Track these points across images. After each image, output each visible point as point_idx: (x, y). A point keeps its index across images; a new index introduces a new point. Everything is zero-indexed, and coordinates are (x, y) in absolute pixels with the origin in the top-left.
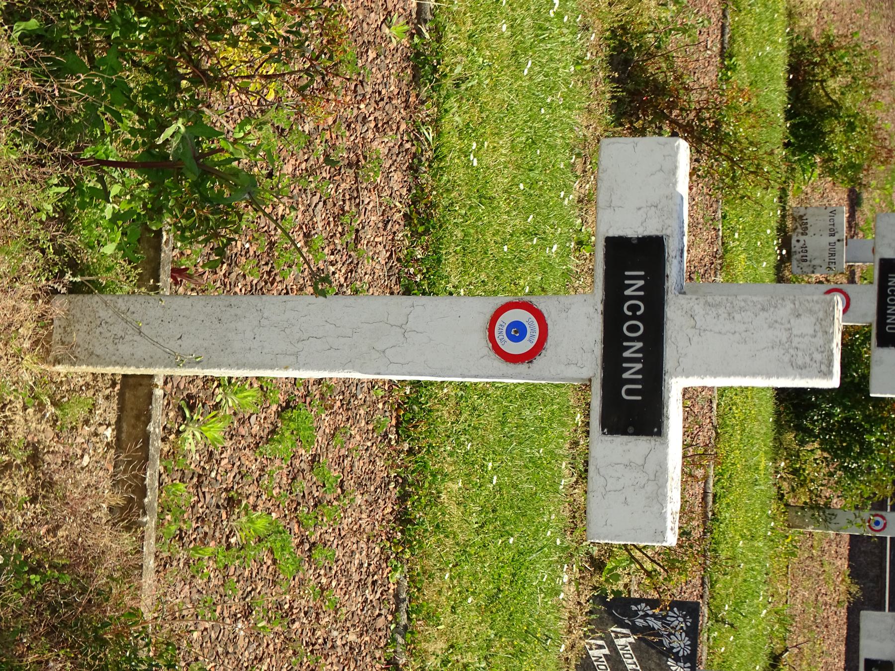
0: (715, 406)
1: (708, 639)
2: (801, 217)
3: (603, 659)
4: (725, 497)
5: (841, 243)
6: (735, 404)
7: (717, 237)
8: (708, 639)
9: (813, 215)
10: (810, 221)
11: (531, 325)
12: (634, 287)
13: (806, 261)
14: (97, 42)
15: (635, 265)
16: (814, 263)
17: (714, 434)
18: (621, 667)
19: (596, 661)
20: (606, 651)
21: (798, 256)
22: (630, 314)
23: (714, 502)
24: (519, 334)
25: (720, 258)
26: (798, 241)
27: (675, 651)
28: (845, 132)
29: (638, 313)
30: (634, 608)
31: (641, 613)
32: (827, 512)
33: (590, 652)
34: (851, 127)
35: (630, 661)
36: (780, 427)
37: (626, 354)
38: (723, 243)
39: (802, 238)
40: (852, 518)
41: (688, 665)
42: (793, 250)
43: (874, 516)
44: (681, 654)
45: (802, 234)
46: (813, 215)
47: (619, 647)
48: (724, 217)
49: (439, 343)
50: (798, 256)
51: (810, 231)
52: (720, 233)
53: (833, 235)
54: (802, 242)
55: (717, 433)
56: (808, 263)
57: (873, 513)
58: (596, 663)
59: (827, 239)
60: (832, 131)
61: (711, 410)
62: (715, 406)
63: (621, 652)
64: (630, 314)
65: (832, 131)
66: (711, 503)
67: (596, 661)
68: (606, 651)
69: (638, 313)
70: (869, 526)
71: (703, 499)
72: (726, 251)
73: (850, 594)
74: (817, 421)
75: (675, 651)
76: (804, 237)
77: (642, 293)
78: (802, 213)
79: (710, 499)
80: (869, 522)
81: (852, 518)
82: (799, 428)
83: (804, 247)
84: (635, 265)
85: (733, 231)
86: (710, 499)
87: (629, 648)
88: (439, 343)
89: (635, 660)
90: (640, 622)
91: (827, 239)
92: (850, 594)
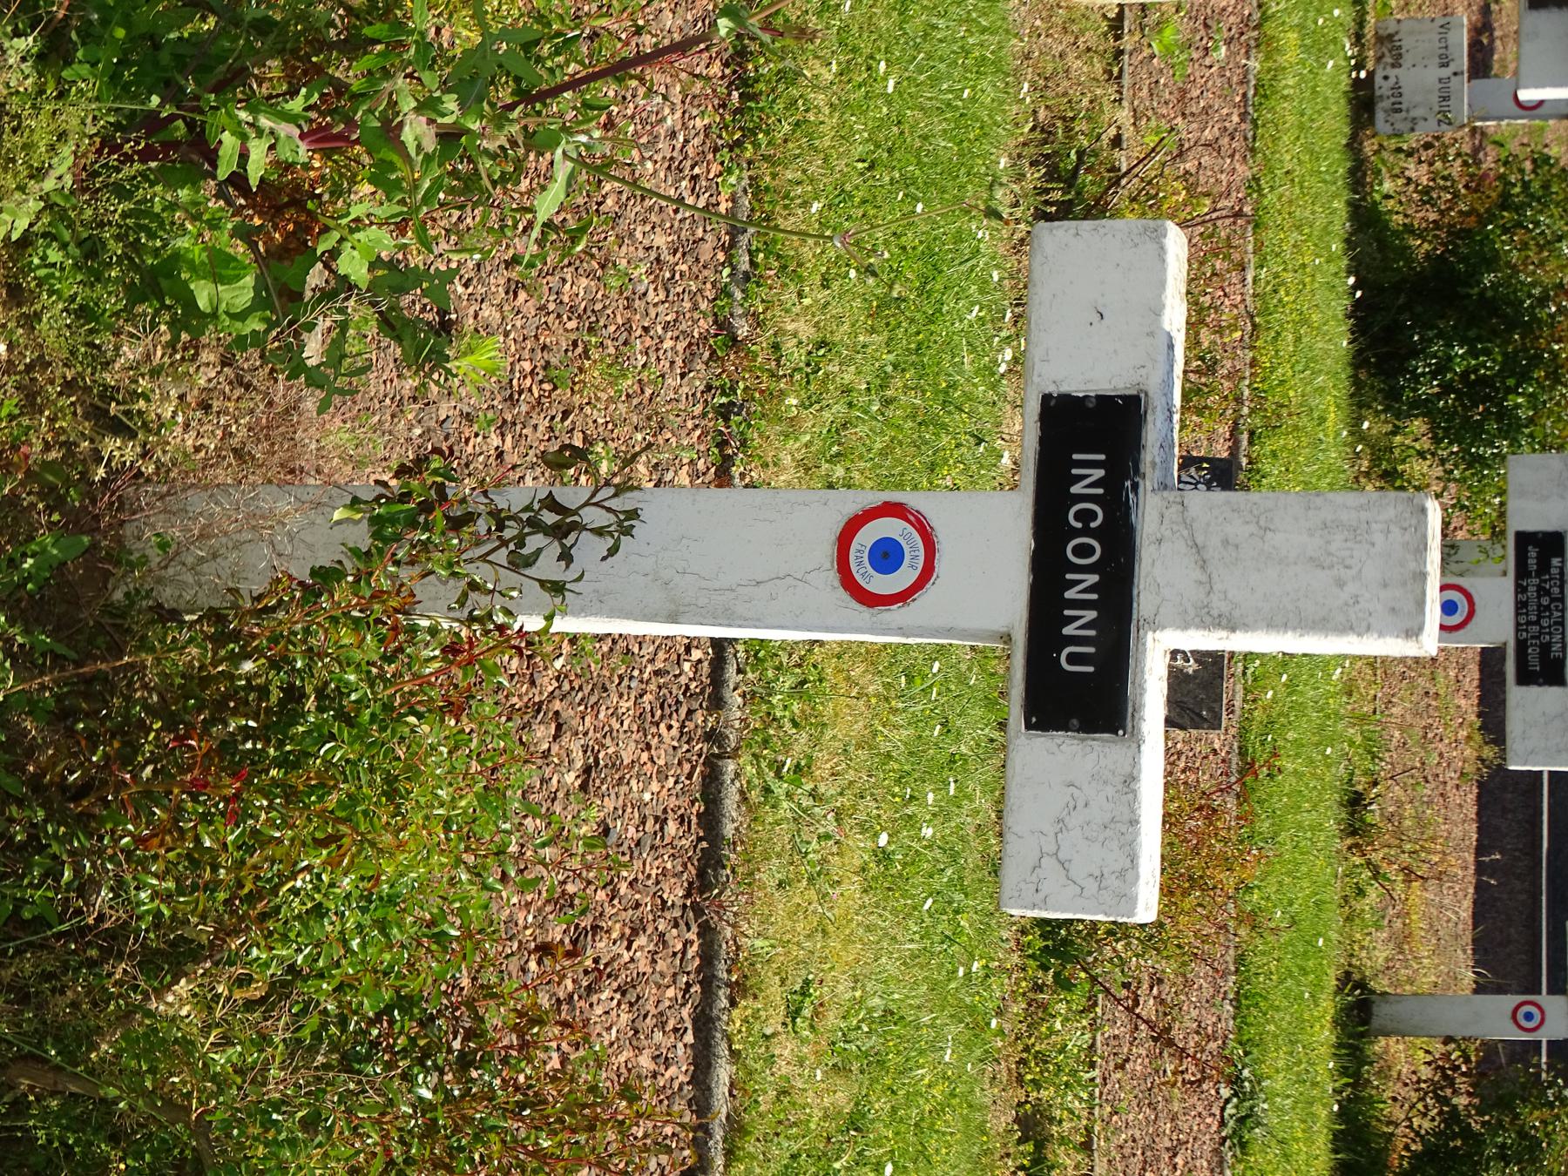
1: (1244, 674)
2: (1390, 37)
5: (1458, 78)
6: (1283, 283)
8: (1244, 674)
9: (1411, 33)
10: (1407, 43)
11: (909, 539)
12: (1088, 479)
13: (1400, 110)
14: (432, 1153)
16: (1413, 114)
21: (1386, 104)
22: (1079, 525)
23: (1251, 443)
24: (879, 559)
25: (1255, 28)
26: (1386, 78)
29: (1093, 525)
36: (1359, 402)
37: (1070, 594)
39: (1392, 73)
42: (1378, 93)
45: (1393, 66)
46: (1411, 33)
50: (1386, 104)
51: (1407, 61)
53: (1445, 65)
54: (1392, 80)
55: (1254, 326)
56: (1403, 114)
59: (1433, 73)
64: (1079, 525)
66: (1245, 443)
69: (1093, 525)
73: (1483, 761)
74: (1423, 374)
76: (1396, 71)
77: (1100, 491)
78: (1391, 31)
82: (1392, 397)
83: (1397, 87)
84: (1089, 438)
91: (1433, 73)
92: (1483, 761)
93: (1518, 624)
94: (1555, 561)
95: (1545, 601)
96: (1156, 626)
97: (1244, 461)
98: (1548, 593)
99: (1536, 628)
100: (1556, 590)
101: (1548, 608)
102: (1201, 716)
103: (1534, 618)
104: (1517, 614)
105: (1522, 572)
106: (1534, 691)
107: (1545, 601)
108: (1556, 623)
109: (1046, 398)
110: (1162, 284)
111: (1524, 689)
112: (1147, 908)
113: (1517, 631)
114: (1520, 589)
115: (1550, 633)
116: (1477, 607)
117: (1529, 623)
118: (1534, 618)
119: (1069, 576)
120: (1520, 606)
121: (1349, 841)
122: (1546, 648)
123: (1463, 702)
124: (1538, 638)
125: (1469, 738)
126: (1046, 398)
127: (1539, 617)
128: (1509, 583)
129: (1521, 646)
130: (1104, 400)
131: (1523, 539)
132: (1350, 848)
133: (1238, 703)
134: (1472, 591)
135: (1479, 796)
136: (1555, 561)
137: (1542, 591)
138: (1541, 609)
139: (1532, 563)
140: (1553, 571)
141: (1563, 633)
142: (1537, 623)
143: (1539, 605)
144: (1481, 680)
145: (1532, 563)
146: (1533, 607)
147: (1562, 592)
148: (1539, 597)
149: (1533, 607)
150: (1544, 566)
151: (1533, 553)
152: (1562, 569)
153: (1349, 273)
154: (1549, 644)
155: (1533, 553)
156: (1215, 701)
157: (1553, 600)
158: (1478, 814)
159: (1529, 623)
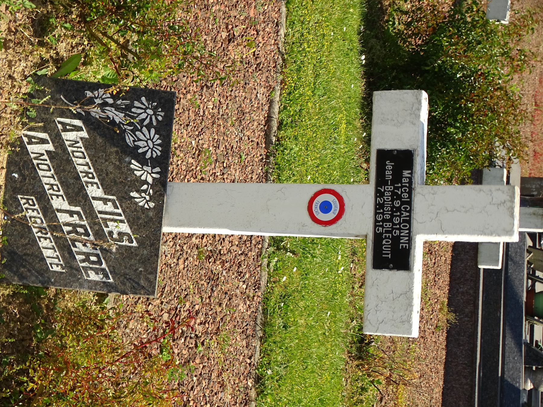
1: (268, 265)
3: (46, 157)
8: (268, 265)
15: (394, 167)
17: (281, 61)
18: (68, 168)
19: (36, 158)
20: (50, 147)
23: (279, 128)
24: (326, 208)
27: (140, 151)
30: (89, 94)
31: (98, 101)
33: (29, 147)
35: (81, 161)
41: (158, 169)
44: (148, 155)
47: (67, 143)
58: (35, 162)
63: (70, 149)
67: (36, 158)
68: (50, 147)
75: (140, 151)
79: (275, 125)
84: (394, 167)
86: (275, 125)
87: (80, 144)
89: (87, 160)
90: (95, 112)
93: (376, 221)
94: (406, 173)
95: (397, 204)
97: (274, 139)
98: (399, 197)
99: (389, 225)
100: (406, 195)
101: (399, 209)
102: (138, 284)
103: (388, 217)
104: (376, 213)
105: (381, 181)
106: (386, 273)
107: (397, 204)
108: (404, 221)
111: (378, 272)
113: (375, 226)
114: (379, 194)
115: (400, 229)
116: (346, 207)
117: (384, 220)
118: (388, 217)
120: (379, 207)
121: (356, 363)
122: (396, 240)
123: (438, 292)
124: (390, 232)
125: (441, 309)
127: (392, 216)
128: (370, 189)
129: (378, 239)
131: (383, 155)
132: (358, 366)
133: (263, 283)
134: (342, 194)
135: (447, 338)
136: (406, 173)
137: (395, 196)
138: (395, 210)
139: (389, 174)
140: (404, 180)
141: (409, 229)
142: (390, 220)
143: (393, 207)
144: (450, 281)
145: (389, 174)
146: (387, 208)
147: (410, 197)
148: (392, 201)
149: (387, 208)
150: (397, 177)
151: (389, 166)
152: (410, 179)
153: (361, 53)
154: (398, 238)
155: (389, 166)
156: (151, 273)
157: (403, 203)
158: (446, 346)
159: (384, 220)
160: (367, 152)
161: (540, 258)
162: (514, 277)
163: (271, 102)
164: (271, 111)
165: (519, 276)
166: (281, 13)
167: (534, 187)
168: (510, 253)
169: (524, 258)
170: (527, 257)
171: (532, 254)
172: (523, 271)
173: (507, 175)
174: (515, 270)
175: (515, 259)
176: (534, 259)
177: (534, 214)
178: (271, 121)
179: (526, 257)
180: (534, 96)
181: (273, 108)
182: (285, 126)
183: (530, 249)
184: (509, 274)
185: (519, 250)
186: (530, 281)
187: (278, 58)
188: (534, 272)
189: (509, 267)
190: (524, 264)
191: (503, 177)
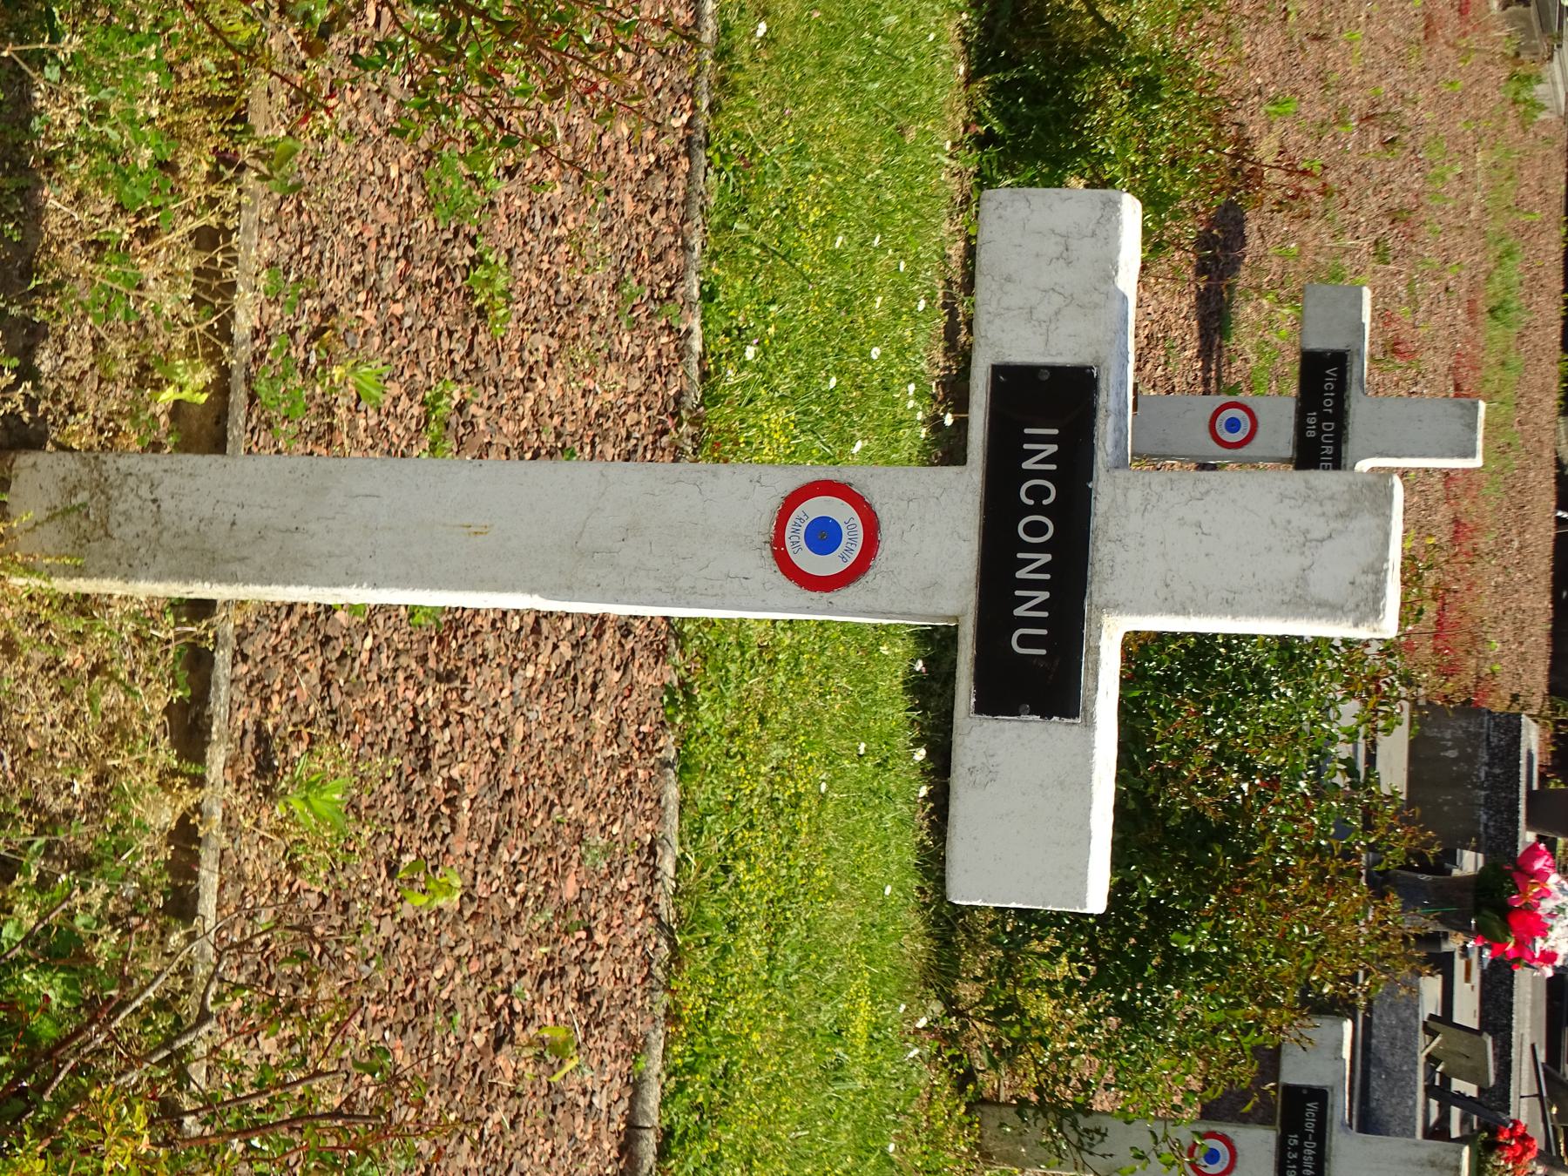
0: (668, 865)
4: (700, 1136)
7: (682, 353)
11: (852, 530)
12: (1040, 455)
15: (1035, 443)
17: (665, 951)
22: (1031, 502)
23: (663, 1153)
24: (823, 539)
28: (1133, 106)
29: (1045, 502)
32: (1083, 1123)
34: (1147, 89)
37: (1021, 574)
38: (705, 375)
40: (1146, 1144)
43: (1204, 1136)
48: (708, 296)
49: (686, 548)
52: (697, 346)
57: (1203, 1128)
60: (1099, 101)
61: (653, 875)
62: (668, 865)
64: (1031, 502)
65: (1099, 101)
69: (1045, 502)
70: (1193, 1166)
71: (622, 1149)
72: (711, 397)
79: (649, 1145)
80: (1191, 1153)
81: (1146, 1144)
84: (1046, 411)
85: (738, 335)
86: (649, 1145)
88: (686, 548)
96: (1117, 607)
109: (998, 370)
110: (1141, 612)
112: (1096, 902)
119: (1054, 467)
126: (998, 370)
130: (1057, 372)
160: (955, 390)
161: (1463, 1050)
162: (1389, 1111)
163: (636, 1086)
164: (638, 1108)
165: (1401, 1108)
166: (664, 809)
167: (1448, 735)
168: (1374, 1041)
169: (1415, 1054)
170: (1424, 1046)
171: (1438, 1039)
172: (1414, 1093)
173: (1367, 750)
174: (1391, 1090)
175: (1389, 1059)
176: (1445, 1051)
177: (1433, 1164)
178: (638, 1139)
179: (1421, 1044)
180: (1452, 370)
181: (644, 1101)
182: (681, 1143)
183: (1432, 1025)
184: (1373, 1104)
185: (1400, 1032)
186: (1434, 1103)
187: (657, 946)
188: (1446, 1080)
189: (1374, 1084)
190: (1414, 1071)
191: (1339, 1047)
